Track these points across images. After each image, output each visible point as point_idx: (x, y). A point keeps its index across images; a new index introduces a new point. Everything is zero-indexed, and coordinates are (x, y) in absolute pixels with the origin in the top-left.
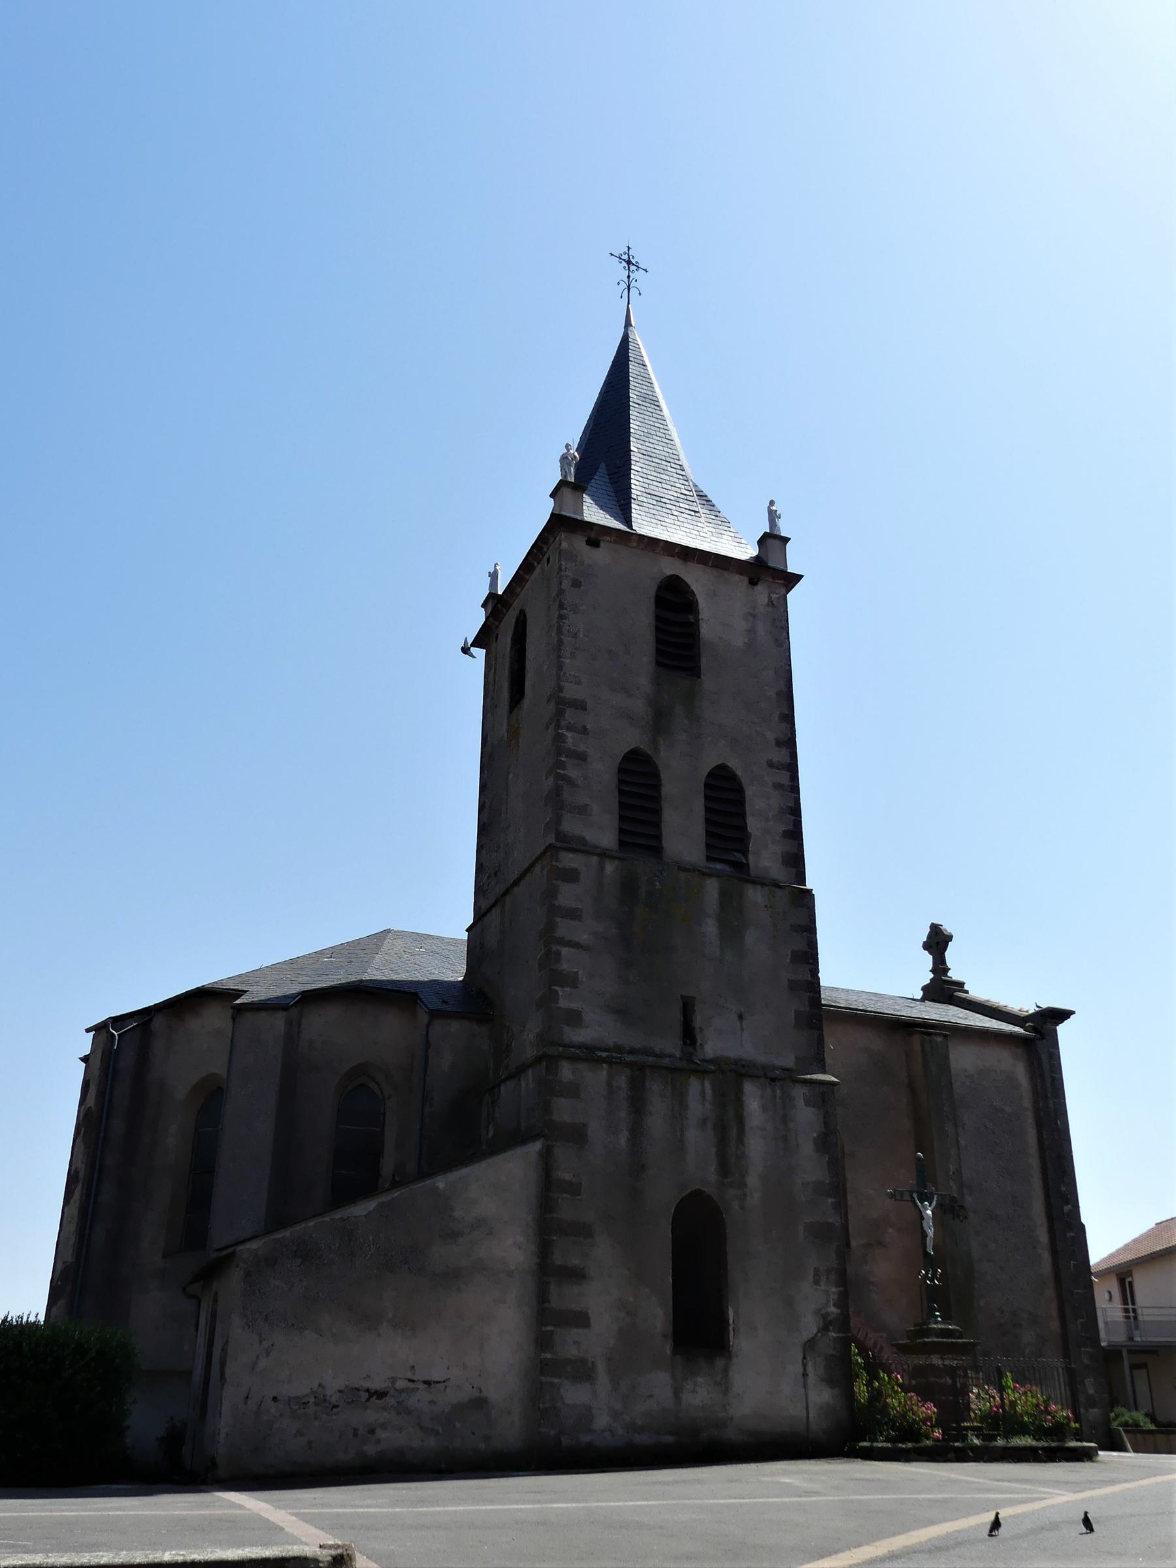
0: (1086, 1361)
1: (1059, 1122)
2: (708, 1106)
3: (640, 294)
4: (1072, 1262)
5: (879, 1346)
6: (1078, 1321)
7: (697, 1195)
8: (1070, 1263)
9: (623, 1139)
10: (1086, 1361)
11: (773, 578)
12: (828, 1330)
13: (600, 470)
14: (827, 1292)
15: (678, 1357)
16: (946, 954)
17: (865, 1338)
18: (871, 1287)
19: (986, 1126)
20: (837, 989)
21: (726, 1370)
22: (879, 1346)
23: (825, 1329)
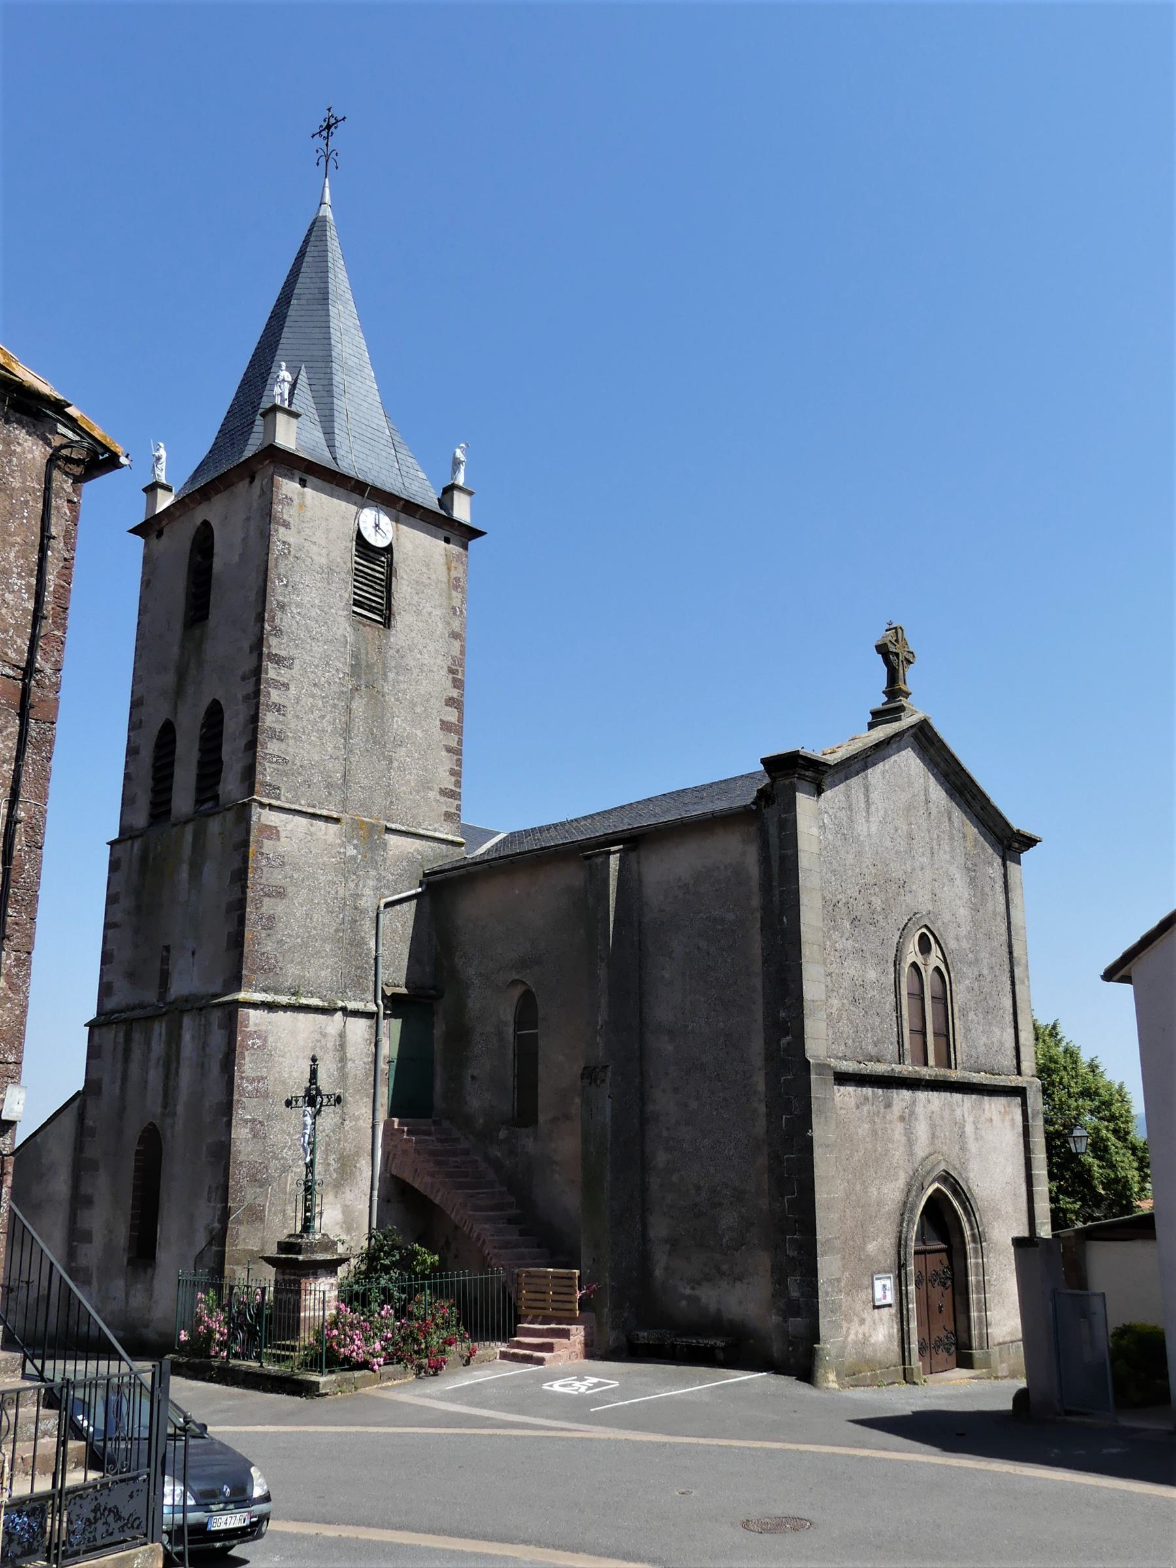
0: (791, 1253)
1: (785, 920)
2: (162, 1045)
3: (337, 168)
4: (784, 1117)
5: (482, 1239)
6: (786, 1197)
7: (151, 1124)
8: (782, 1118)
9: (117, 1090)
10: (791, 1253)
11: (262, 464)
12: (212, 1245)
13: (256, 423)
14: (214, 1208)
15: (130, 1267)
16: (886, 669)
17: (470, 1232)
18: (554, 1167)
19: (698, 948)
20: (541, 830)
21: (152, 1278)
22: (482, 1239)
23: (210, 1243)
